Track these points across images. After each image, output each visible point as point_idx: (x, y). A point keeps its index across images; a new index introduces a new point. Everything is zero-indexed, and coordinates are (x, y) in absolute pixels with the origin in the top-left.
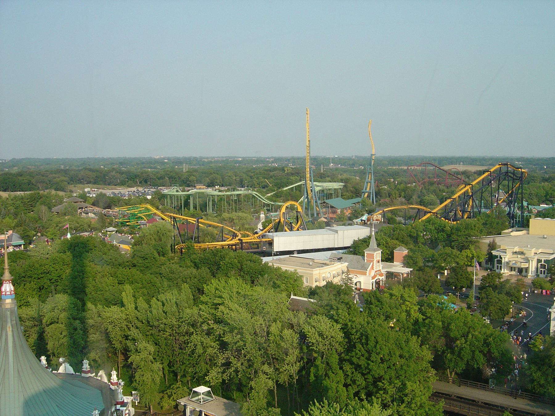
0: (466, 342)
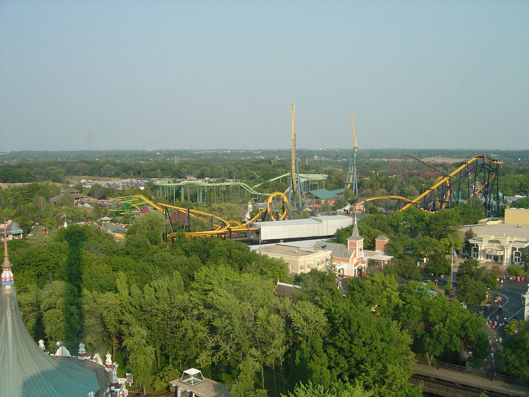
0: (444, 326)
